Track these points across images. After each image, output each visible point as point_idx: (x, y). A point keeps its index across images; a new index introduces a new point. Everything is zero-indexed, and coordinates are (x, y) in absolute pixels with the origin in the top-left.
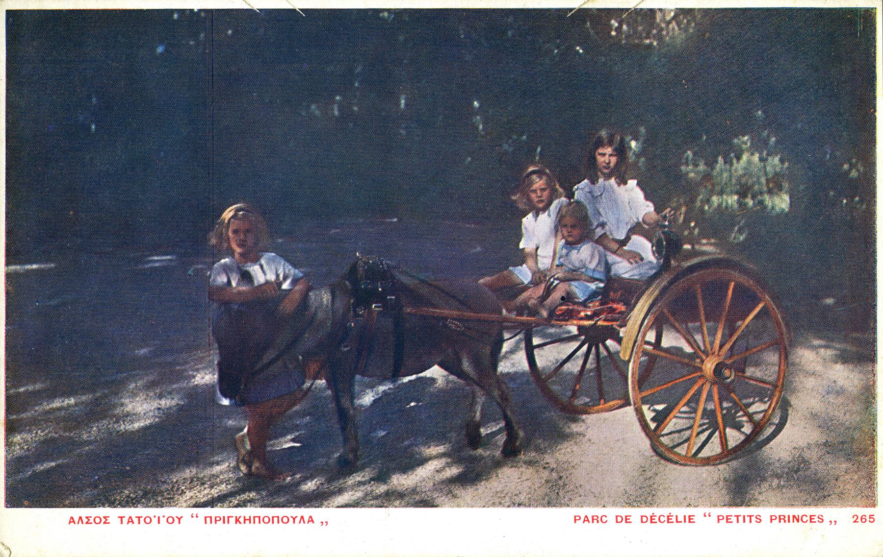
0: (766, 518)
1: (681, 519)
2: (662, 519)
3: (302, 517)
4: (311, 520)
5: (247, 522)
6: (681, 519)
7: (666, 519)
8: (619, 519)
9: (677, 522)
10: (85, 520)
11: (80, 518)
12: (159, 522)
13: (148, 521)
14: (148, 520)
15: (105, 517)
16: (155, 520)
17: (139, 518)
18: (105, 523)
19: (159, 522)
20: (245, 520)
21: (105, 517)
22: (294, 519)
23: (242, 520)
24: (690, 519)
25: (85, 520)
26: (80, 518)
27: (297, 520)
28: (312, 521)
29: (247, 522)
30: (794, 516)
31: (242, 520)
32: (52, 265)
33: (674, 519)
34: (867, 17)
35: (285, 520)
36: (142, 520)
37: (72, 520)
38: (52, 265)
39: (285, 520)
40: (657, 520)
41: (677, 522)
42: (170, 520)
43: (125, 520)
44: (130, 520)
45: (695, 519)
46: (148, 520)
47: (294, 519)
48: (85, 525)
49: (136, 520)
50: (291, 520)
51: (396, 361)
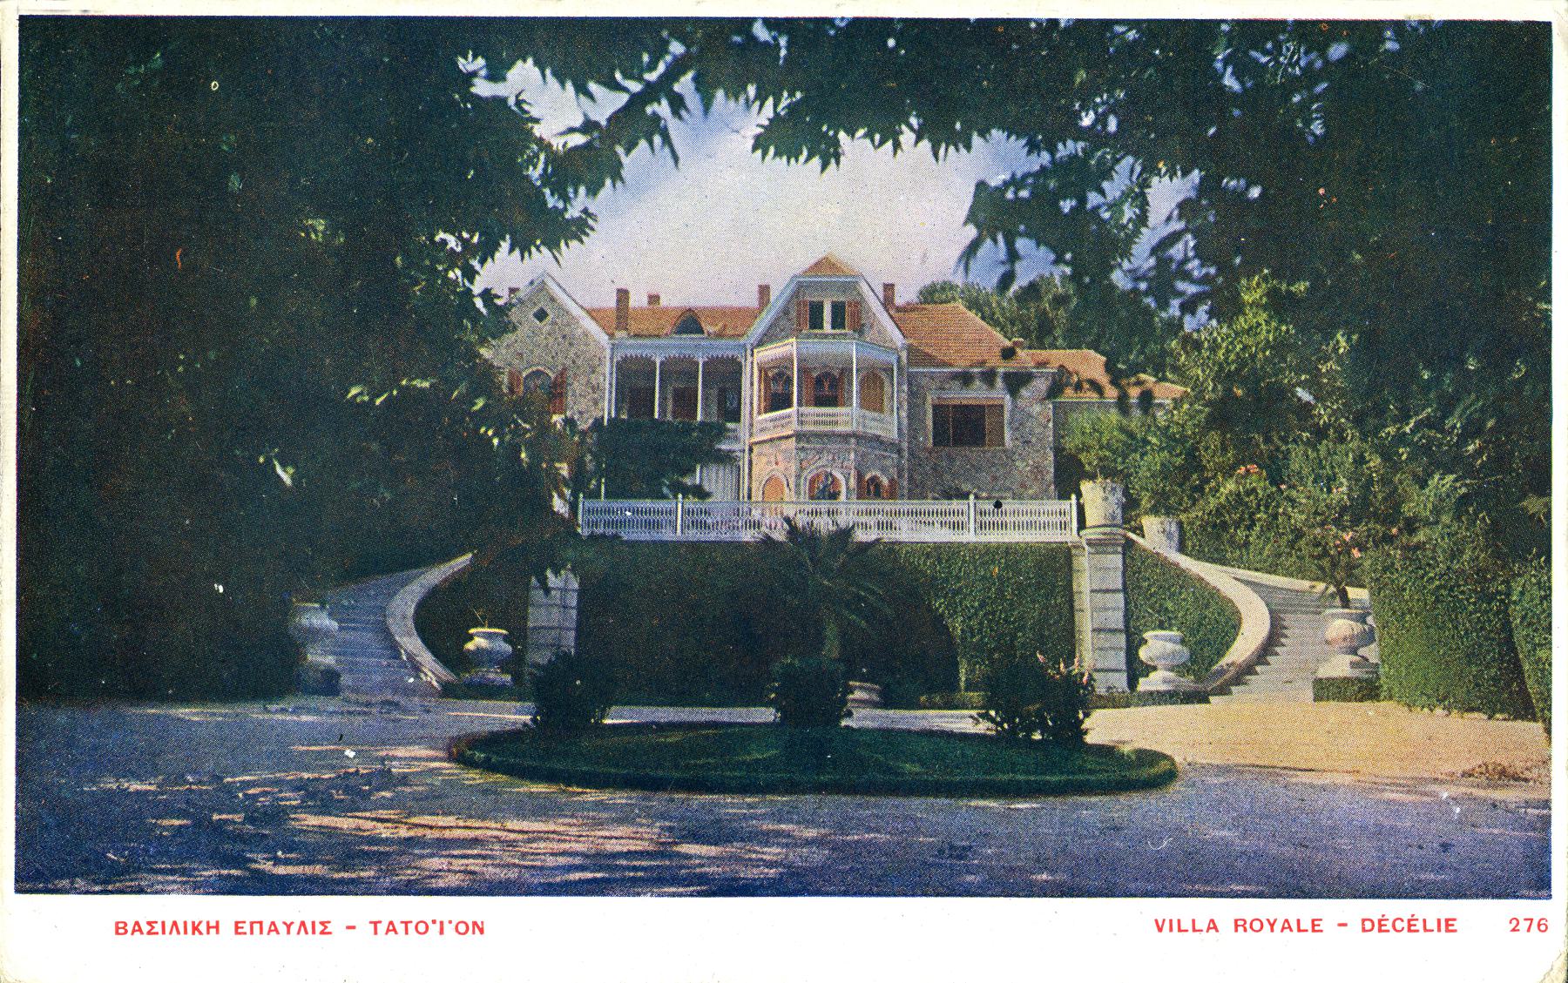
0: (1226, 925)
1: (1432, 925)
2: (1399, 925)
3: (303, 923)
4: (1213, 926)
5: (213, 931)
6: (1432, 925)
7: (1405, 924)
8: (1368, 925)
9: (1194, 930)
10: (146, 928)
11: (175, 923)
12: (442, 932)
13: (422, 928)
14: (422, 928)
15: (149, 923)
16: (435, 928)
17: (406, 923)
18: (322, 933)
19: (442, 932)
20: (209, 928)
21: (149, 923)
22: (1272, 925)
23: (203, 928)
24: (1448, 925)
25: (146, 928)
26: (175, 923)
27: (1278, 927)
28: (1215, 928)
29: (213, 931)
30: (475, 923)
31: (203, 928)
32: (464, 560)
33: (1419, 925)
34: (1526, 46)
35: (1257, 925)
36: (411, 927)
37: (120, 928)
38: (464, 560)
39: (1257, 925)
40: (1389, 926)
41: (1194, 930)
42: (462, 928)
43: (382, 928)
44: (391, 928)
45: (1457, 925)
46: (422, 928)
47: (1272, 925)
48: (145, 936)
49: (400, 928)
50: (1267, 927)
51: (1118, 783)
